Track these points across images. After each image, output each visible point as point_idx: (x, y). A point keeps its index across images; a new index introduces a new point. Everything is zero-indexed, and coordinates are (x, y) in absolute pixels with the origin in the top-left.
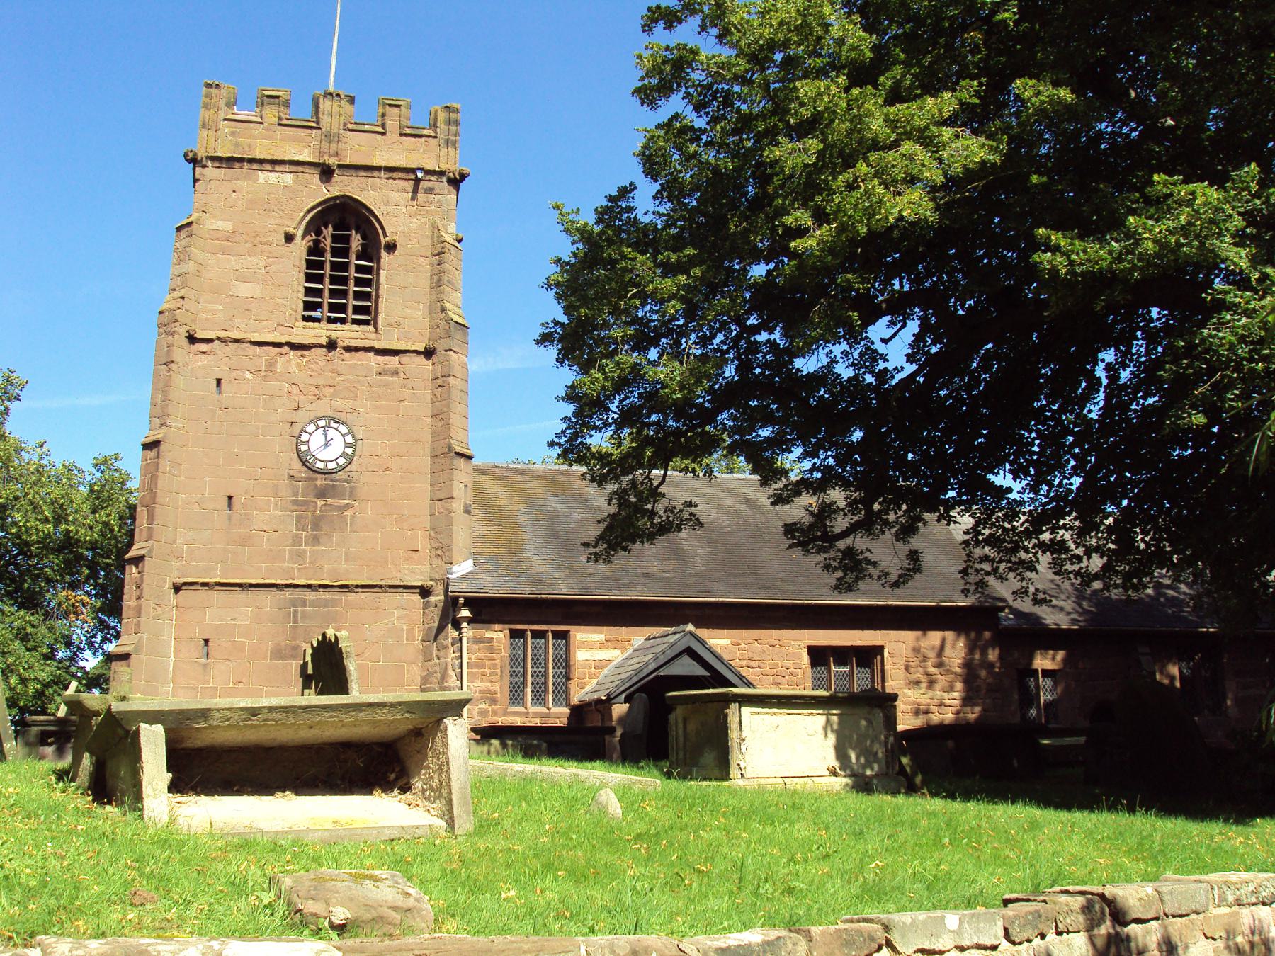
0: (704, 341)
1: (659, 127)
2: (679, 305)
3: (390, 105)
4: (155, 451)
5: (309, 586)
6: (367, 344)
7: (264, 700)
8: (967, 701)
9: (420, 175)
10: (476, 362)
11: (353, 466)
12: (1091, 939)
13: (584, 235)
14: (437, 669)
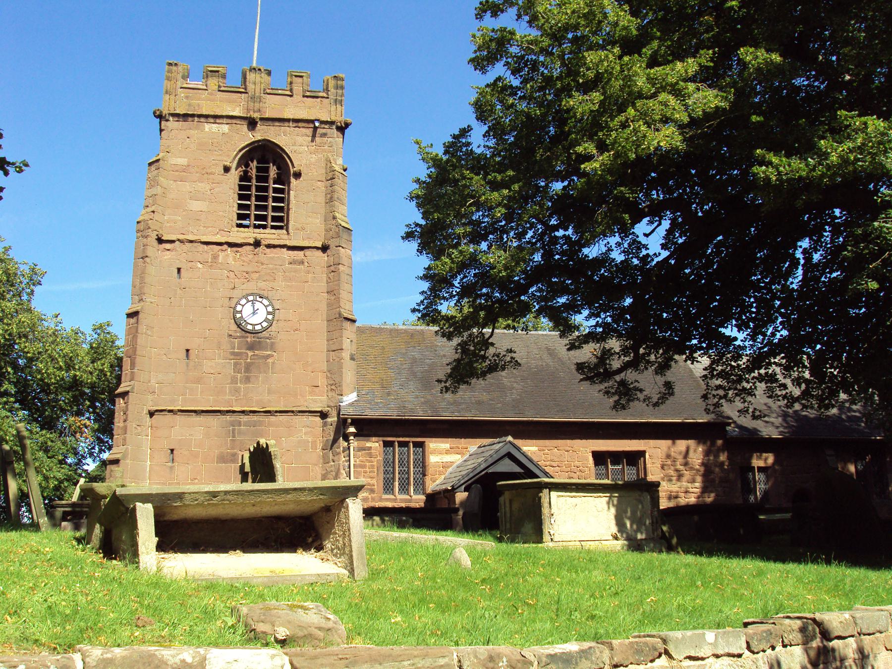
0: (520, 236)
1: (487, 86)
2: (503, 211)
3: (296, 76)
4: (135, 318)
5: (243, 412)
6: (282, 242)
7: (222, 486)
8: (705, 490)
9: (317, 124)
10: (358, 255)
11: (273, 328)
12: (806, 651)
13: (436, 162)
14: (333, 469)
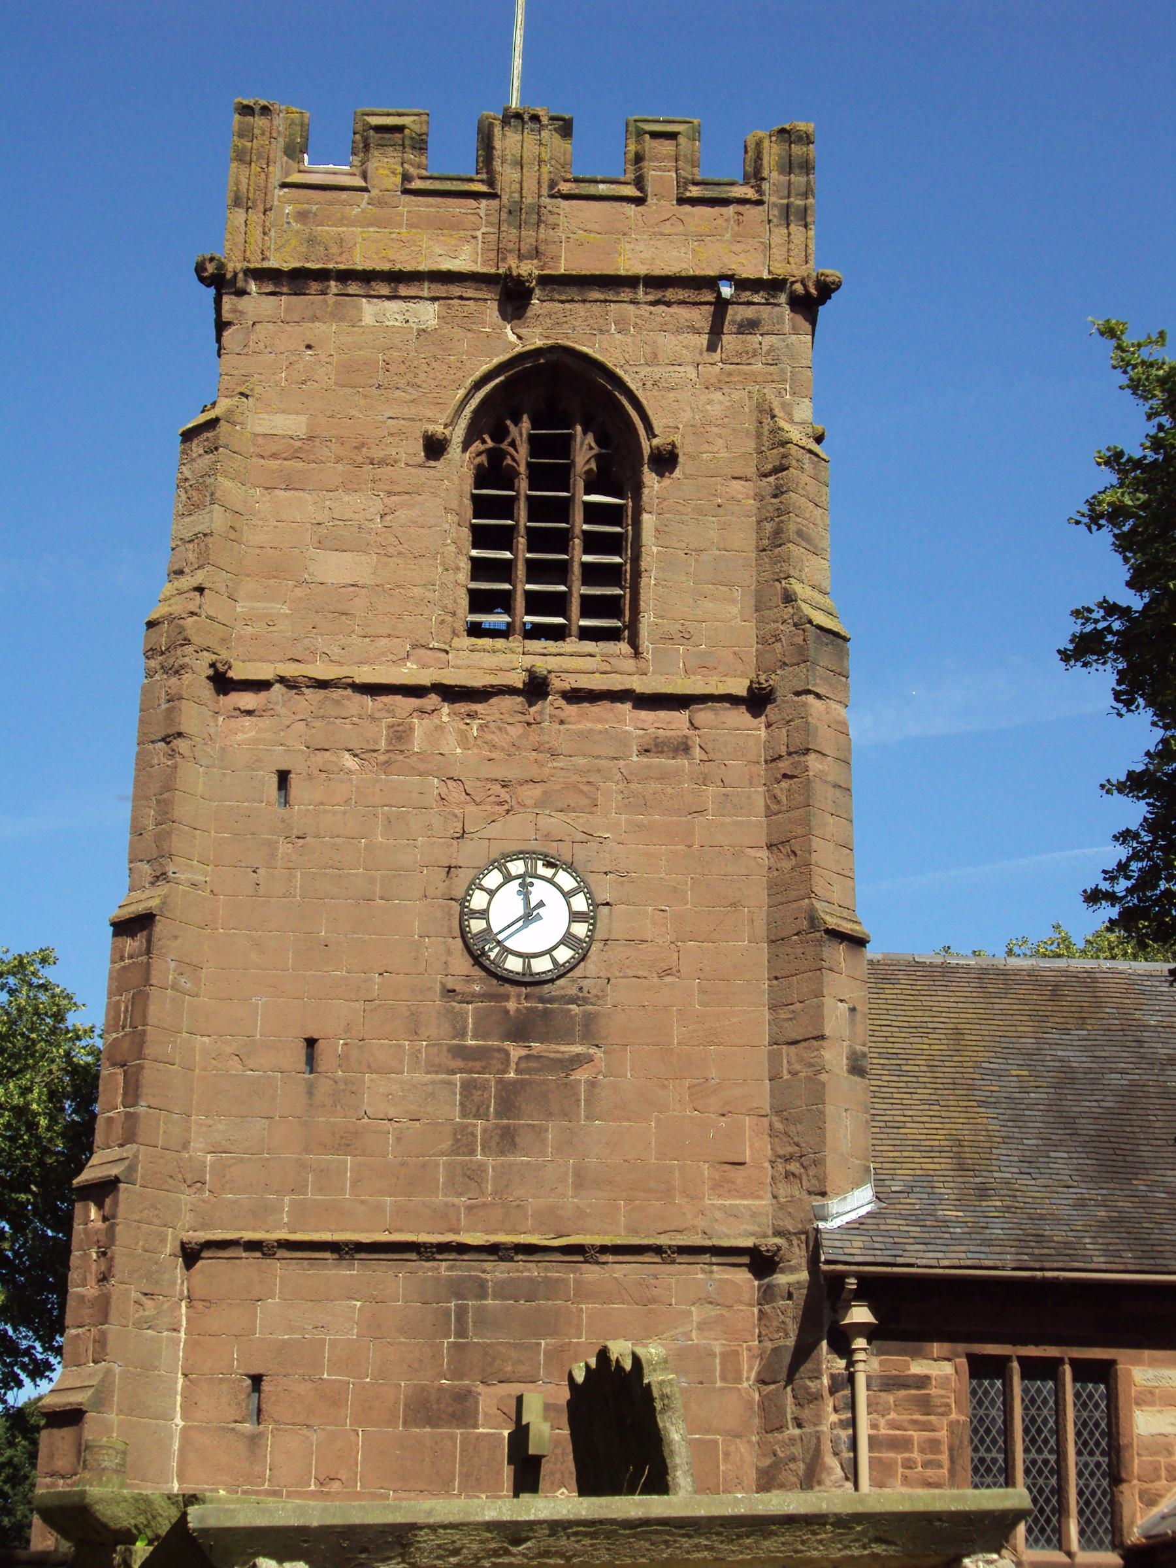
3: (655, 135)
4: (141, 937)
5: (493, 1250)
6: (616, 683)
9: (727, 291)
10: (869, 719)
11: (591, 967)
14: (797, 1450)
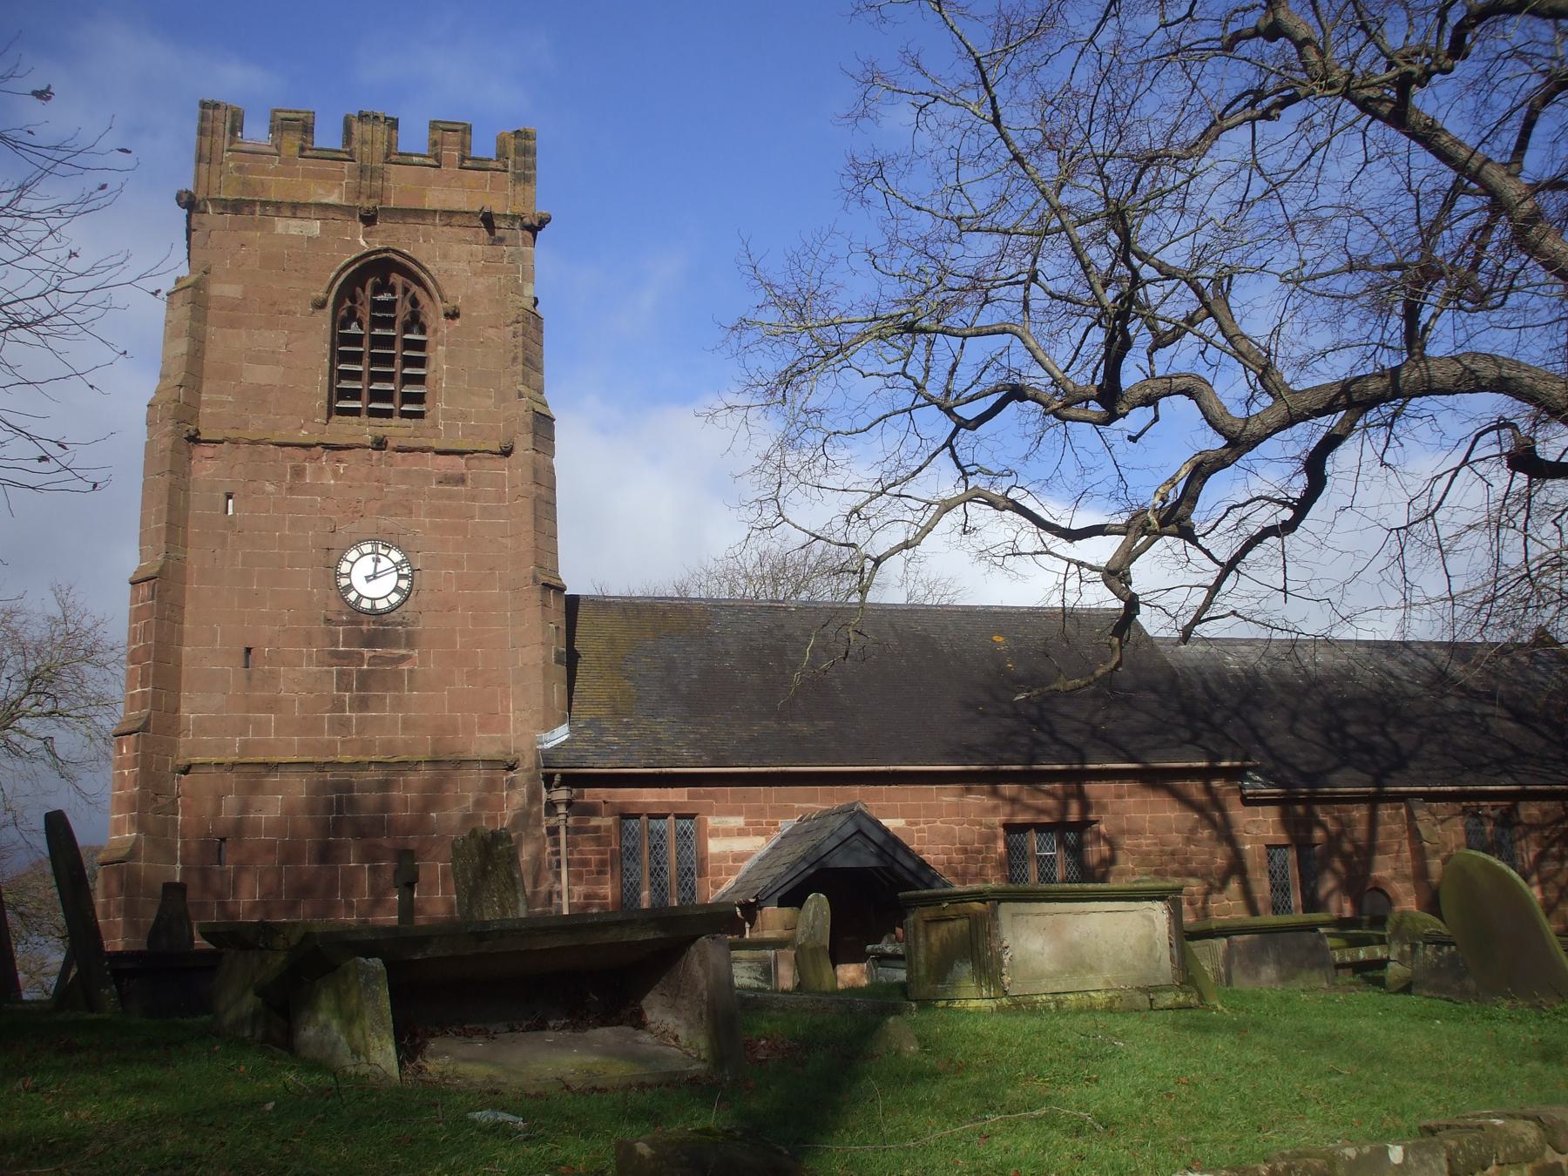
11: (410, 605)
